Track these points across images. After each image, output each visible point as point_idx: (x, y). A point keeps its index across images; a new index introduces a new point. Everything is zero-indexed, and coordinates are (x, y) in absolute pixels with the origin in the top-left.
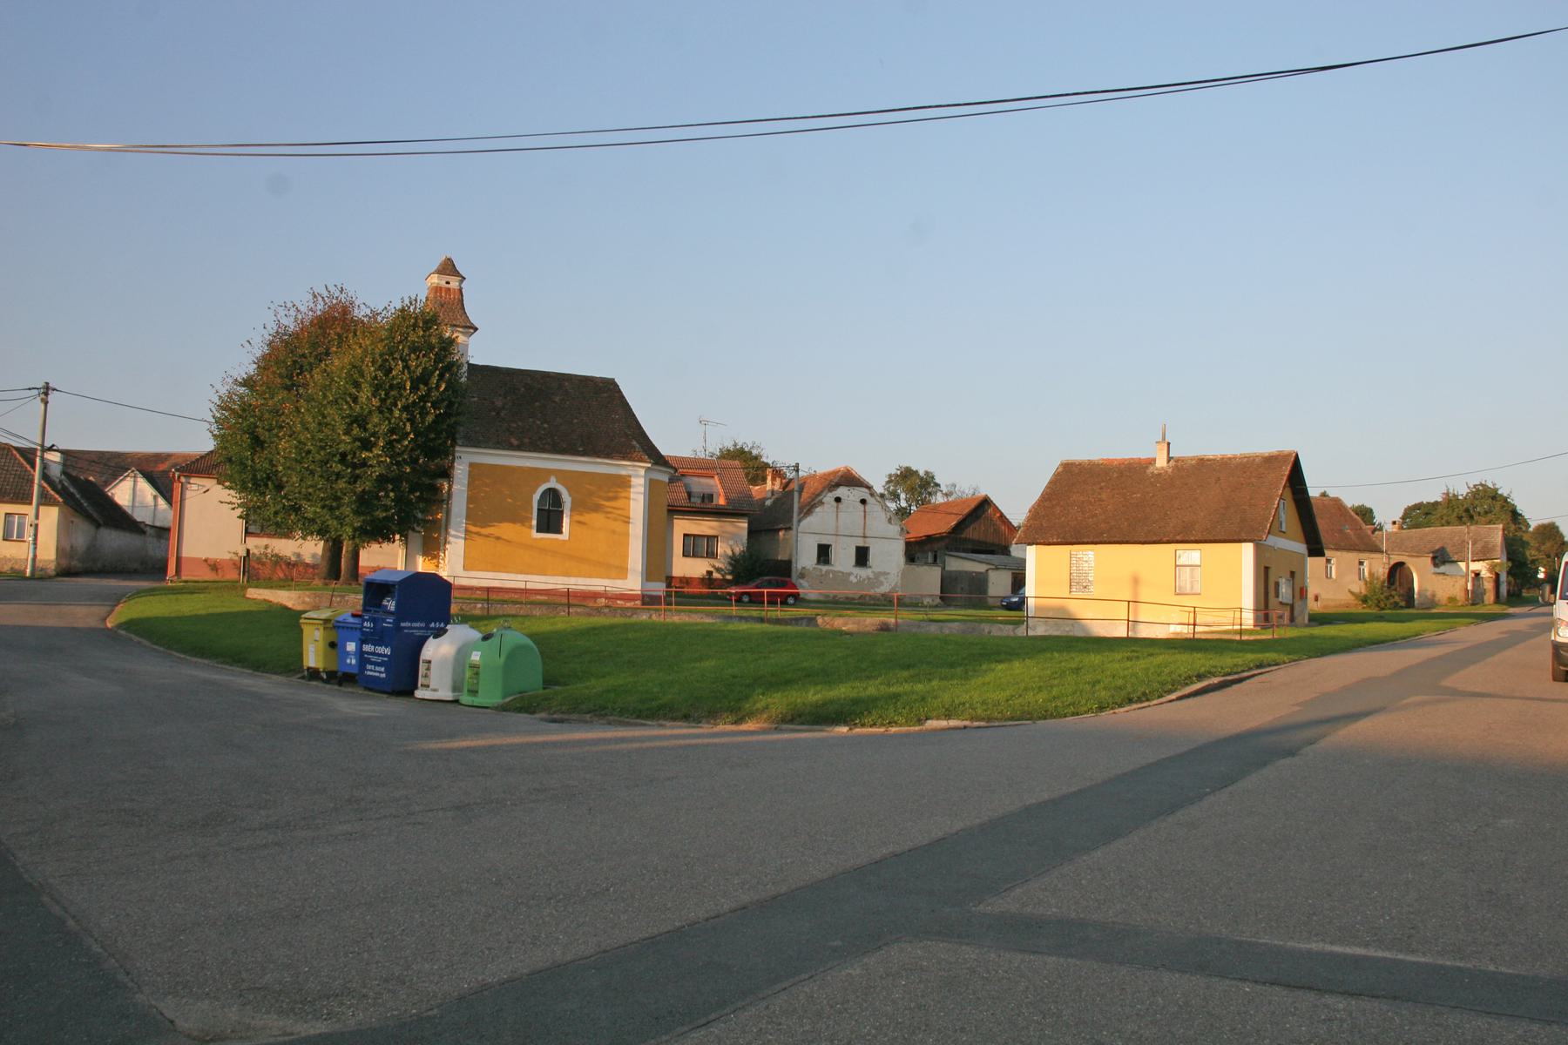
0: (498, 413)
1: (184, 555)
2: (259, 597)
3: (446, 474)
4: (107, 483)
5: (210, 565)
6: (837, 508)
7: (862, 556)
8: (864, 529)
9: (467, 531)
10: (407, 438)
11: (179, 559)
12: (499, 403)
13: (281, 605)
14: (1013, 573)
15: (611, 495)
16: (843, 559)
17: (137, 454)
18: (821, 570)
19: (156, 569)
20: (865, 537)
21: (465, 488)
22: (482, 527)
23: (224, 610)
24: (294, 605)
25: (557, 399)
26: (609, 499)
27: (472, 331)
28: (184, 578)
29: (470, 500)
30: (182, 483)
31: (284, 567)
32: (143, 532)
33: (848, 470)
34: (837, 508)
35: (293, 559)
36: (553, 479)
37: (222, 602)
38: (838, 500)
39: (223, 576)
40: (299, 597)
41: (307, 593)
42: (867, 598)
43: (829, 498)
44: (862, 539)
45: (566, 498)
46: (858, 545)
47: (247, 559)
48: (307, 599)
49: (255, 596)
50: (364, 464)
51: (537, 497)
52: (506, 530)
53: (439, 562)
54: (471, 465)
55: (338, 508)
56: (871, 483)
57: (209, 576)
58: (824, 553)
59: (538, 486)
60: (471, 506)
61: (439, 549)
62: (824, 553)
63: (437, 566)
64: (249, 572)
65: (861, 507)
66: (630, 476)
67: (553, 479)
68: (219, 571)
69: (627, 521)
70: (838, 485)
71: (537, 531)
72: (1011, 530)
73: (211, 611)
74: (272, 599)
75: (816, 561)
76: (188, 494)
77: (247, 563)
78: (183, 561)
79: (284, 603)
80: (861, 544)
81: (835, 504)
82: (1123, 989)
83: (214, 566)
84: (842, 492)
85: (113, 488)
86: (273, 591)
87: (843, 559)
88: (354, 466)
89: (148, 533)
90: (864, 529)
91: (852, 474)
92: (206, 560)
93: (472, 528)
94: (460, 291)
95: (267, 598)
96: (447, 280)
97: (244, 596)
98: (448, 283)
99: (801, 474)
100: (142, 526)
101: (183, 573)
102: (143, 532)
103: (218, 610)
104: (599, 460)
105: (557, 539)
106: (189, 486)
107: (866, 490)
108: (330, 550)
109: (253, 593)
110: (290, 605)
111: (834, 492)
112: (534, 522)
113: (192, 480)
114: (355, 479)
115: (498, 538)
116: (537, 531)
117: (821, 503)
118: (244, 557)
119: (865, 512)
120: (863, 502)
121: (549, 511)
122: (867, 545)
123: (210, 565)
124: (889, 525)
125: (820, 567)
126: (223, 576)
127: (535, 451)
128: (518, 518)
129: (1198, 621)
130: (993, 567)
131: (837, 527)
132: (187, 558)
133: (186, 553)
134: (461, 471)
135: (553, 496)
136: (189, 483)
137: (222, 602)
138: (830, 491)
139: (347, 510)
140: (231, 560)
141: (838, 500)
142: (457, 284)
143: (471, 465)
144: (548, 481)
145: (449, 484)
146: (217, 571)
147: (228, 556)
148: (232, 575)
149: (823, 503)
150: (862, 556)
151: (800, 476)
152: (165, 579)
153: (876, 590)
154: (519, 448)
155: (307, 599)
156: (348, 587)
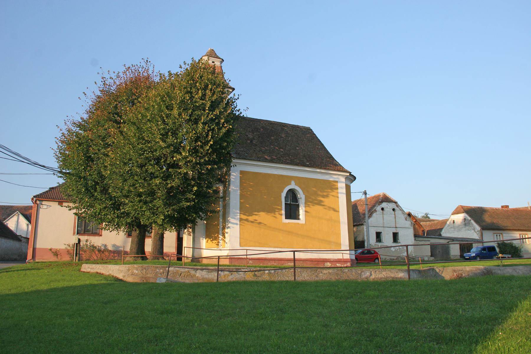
0: (251, 141)
1: (37, 247)
2: (92, 271)
3: (224, 180)
4: (5, 219)
5: (53, 252)
6: (383, 213)
7: (395, 236)
8: (396, 223)
9: (241, 220)
10: (207, 145)
11: (34, 249)
12: (250, 136)
13: (113, 276)
14: (460, 245)
15: (325, 194)
16: (388, 239)
17: (20, 206)
18: (378, 245)
19: (22, 258)
20: (396, 228)
21: (238, 189)
22: (248, 216)
23: (66, 284)
24: (124, 276)
25: (283, 136)
26: (323, 196)
27: (231, 90)
28: (37, 261)
29: (242, 196)
30: (37, 204)
31: (97, 252)
32: (20, 241)
33: (385, 194)
34: (383, 213)
35: (103, 248)
36: (293, 183)
37: (63, 276)
38: (383, 209)
39: (61, 259)
40: (129, 270)
41: (135, 266)
42: (400, 259)
43: (378, 208)
44: (395, 228)
45: (301, 195)
46: (394, 232)
47: (78, 245)
48: (136, 272)
49: (89, 270)
50: (175, 165)
51: (284, 194)
52: (263, 217)
53: (219, 242)
54: (242, 172)
55: (151, 202)
56: (396, 200)
57: (53, 259)
58: (378, 235)
59: (284, 188)
60: (242, 201)
61: (218, 233)
62: (378, 235)
63: (218, 245)
64: (79, 254)
65: (393, 212)
66: (337, 182)
67: (293, 183)
68: (59, 256)
69: (336, 211)
70: (382, 202)
71: (286, 218)
72: (420, 227)
73: (53, 285)
74: (102, 271)
75: (375, 241)
76: (41, 211)
77: (78, 248)
78: (37, 250)
79: (115, 275)
80: (395, 231)
81: (381, 211)
82: (154, 310)
83: (56, 253)
84: (384, 205)
85: (7, 221)
86: (105, 265)
87: (388, 239)
88: (170, 166)
89: (23, 241)
90: (396, 223)
91: (387, 196)
92: (51, 250)
93: (244, 217)
94: (221, 67)
95: (99, 271)
96: (214, 61)
97: (79, 270)
98: (213, 62)
99: (368, 196)
100: (20, 237)
101: (36, 258)
102: (20, 241)
103: (60, 285)
104: (318, 170)
105: (298, 223)
106: (41, 206)
107: (395, 204)
108: (138, 237)
109: (86, 268)
110: (120, 276)
111: (381, 205)
112: (283, 212)
113: (44, 203)
114: (167, 177)
115: (260, 223)
116: (286, 218)
117: (376, 211)
118: (77, 244)
119: (395, 214)
120: (394, 210)
121: (290, 204)
122: (397, 232)
123: (53, 252)
124: (406, 221)
125: (377, 244)
126: (61, 259)
127: (282, 163)
128: (271, 210)
129: (296, 266)
130: (452, 240)
131: (384, 223)
132: (40, 249)
133: (38, 246)
134: (235, 176)
135: (292, 195)
136: (42, 204)
137: (63, 276)
138: (379, 205)
139: (158, 203)
140: (66, 248)
141: (383, 209)
142: (219, 63)
143: (242, 172)
144: (290, 184)
145: (225, 186)
146: (57, 256)
147: (63, 247)
148: (66, 258)
149: (376, 211)
150: (395, 236)
151: (367, 197)
152: (26, 262)
153: (403, 254)
154: (272, 161)
155: (136, 272)
156: (157, 261)
